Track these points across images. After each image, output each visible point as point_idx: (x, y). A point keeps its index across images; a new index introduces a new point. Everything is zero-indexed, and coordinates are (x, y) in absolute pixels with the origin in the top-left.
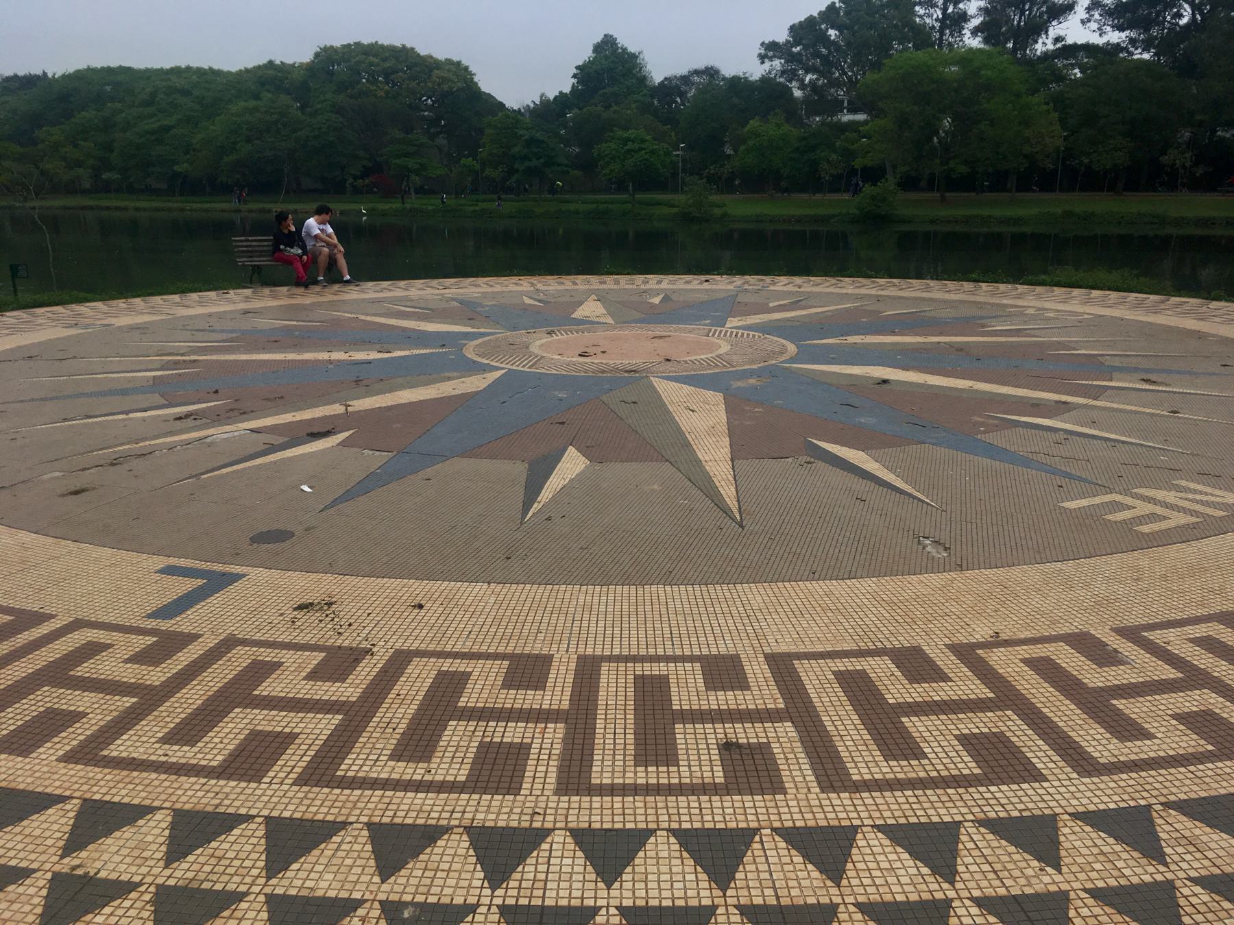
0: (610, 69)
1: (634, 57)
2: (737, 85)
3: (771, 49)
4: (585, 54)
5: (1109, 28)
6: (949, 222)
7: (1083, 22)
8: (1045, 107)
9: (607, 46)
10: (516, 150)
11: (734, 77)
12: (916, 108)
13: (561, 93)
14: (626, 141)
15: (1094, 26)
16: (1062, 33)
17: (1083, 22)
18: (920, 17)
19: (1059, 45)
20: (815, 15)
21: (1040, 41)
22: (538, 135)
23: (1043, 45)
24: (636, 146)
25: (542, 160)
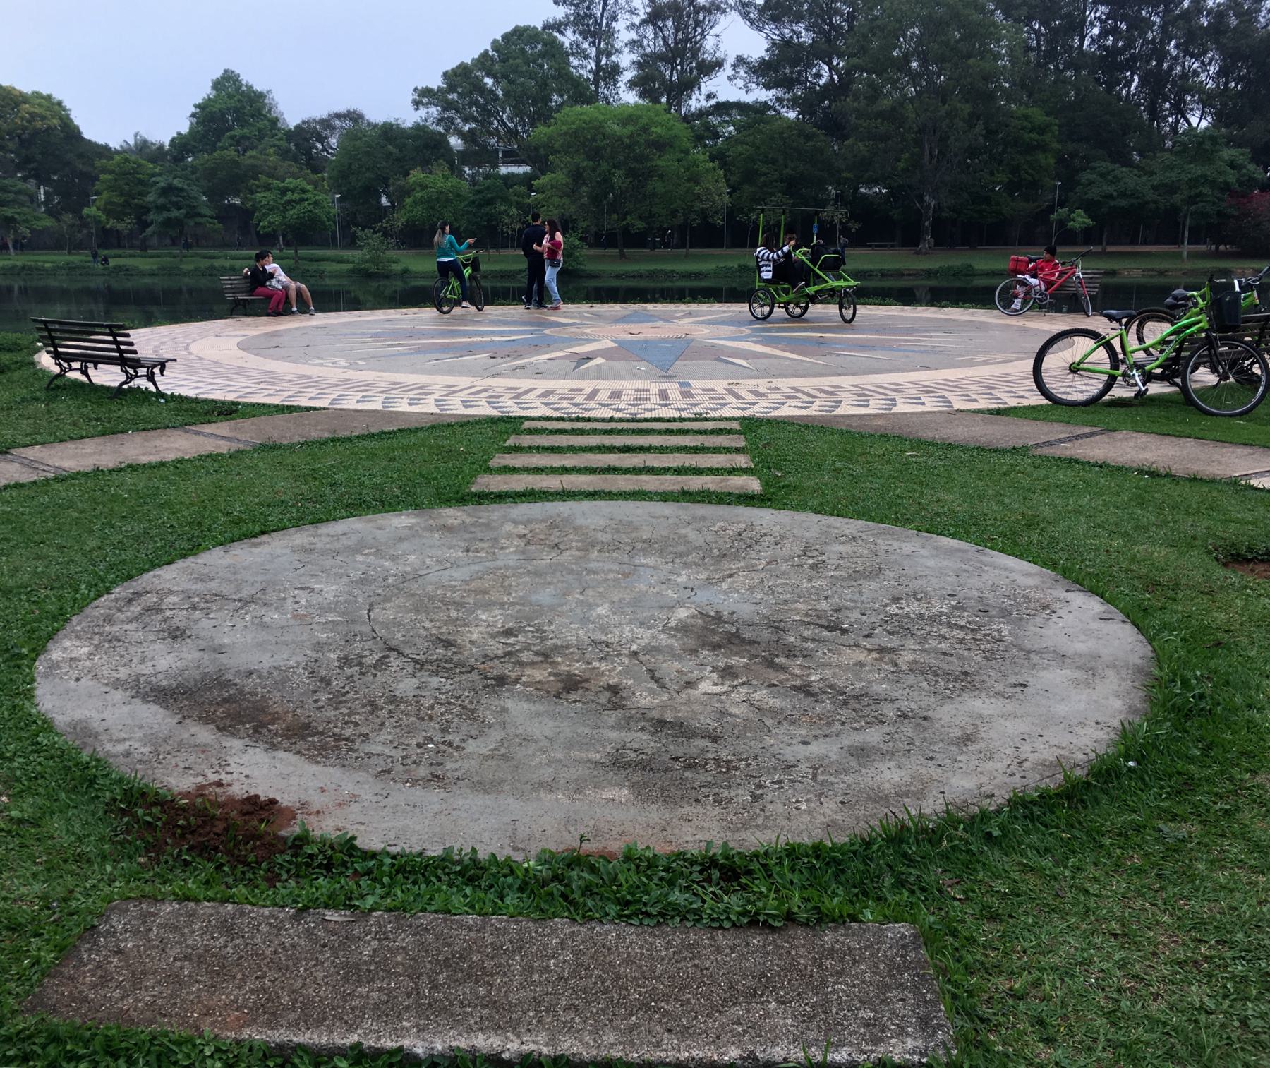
0: (233, 113)
1: (261, 96)
2: (389, 132)
3: (424, 96)
4: (203, 91)
5: (754, 86)
6: (634, 277)
7: (729, 79)
8: (711, 165)
9: (228, 83)
10: (150, 198)
11: (385, 124)
12: (591, 163)
13: (179, 134)
14: (284, 191)
15: (740, 83)
16: (713, 90)
17: (729, 79)
18: (575, 68)
19: (713, 102)
20: (468, 61)
21: (694, 97)
22: (177, 183)
23: (696, 102)
24: (296, 196)
25: (183, 211)
